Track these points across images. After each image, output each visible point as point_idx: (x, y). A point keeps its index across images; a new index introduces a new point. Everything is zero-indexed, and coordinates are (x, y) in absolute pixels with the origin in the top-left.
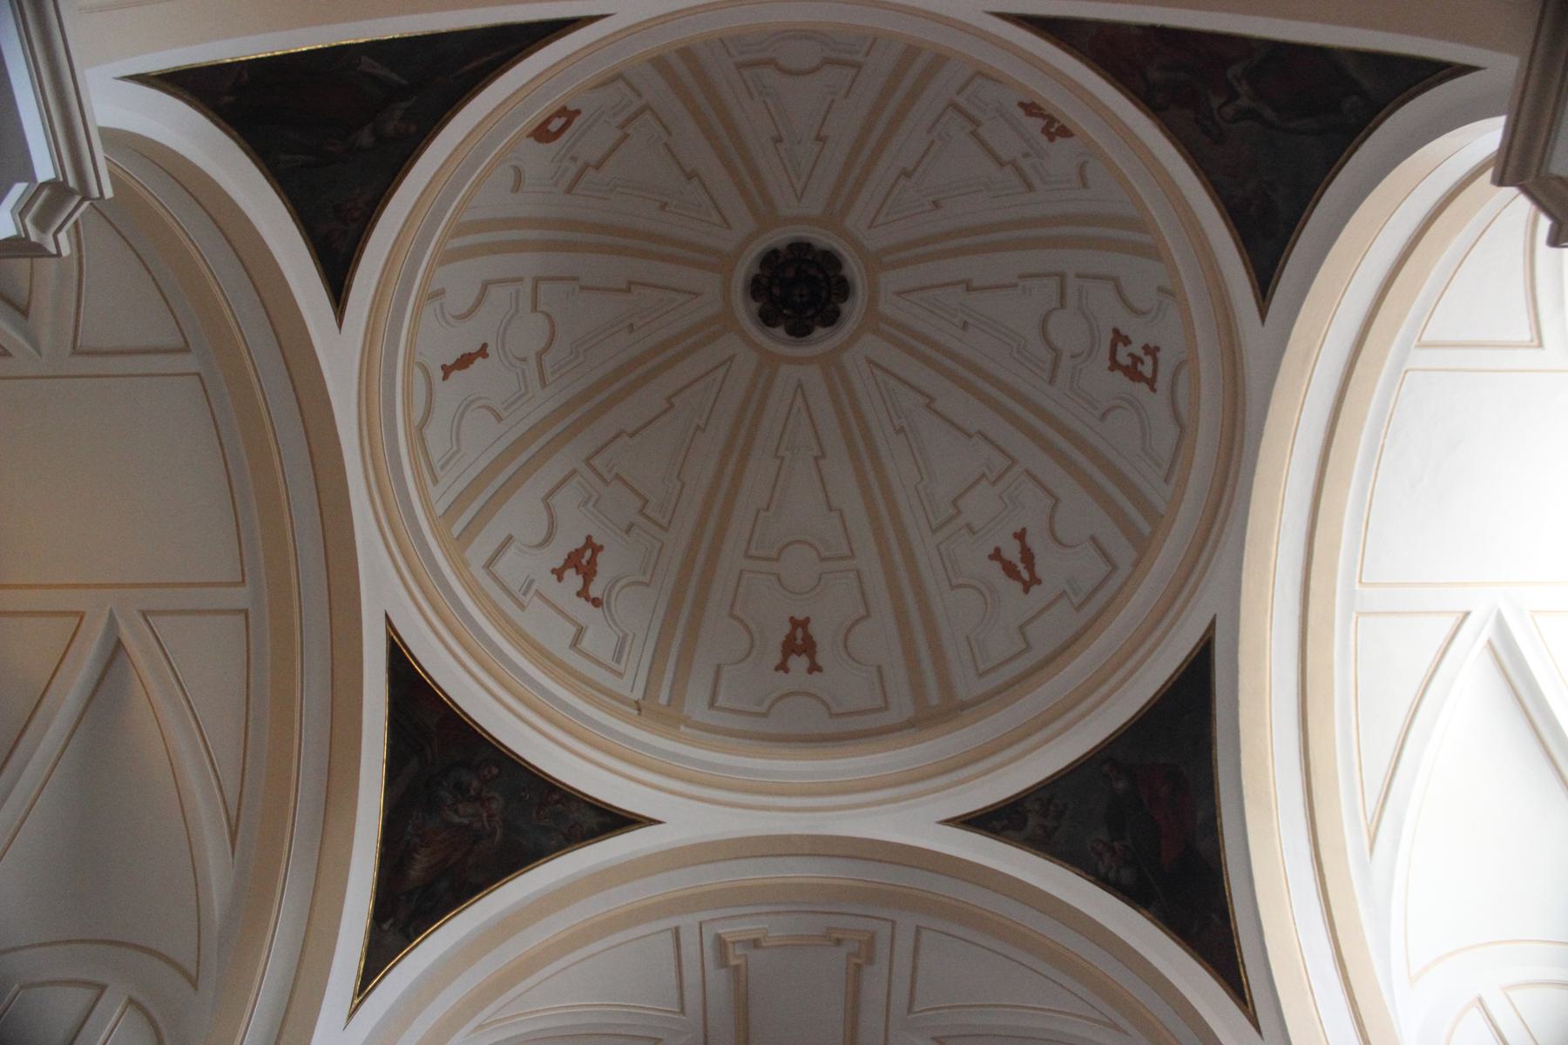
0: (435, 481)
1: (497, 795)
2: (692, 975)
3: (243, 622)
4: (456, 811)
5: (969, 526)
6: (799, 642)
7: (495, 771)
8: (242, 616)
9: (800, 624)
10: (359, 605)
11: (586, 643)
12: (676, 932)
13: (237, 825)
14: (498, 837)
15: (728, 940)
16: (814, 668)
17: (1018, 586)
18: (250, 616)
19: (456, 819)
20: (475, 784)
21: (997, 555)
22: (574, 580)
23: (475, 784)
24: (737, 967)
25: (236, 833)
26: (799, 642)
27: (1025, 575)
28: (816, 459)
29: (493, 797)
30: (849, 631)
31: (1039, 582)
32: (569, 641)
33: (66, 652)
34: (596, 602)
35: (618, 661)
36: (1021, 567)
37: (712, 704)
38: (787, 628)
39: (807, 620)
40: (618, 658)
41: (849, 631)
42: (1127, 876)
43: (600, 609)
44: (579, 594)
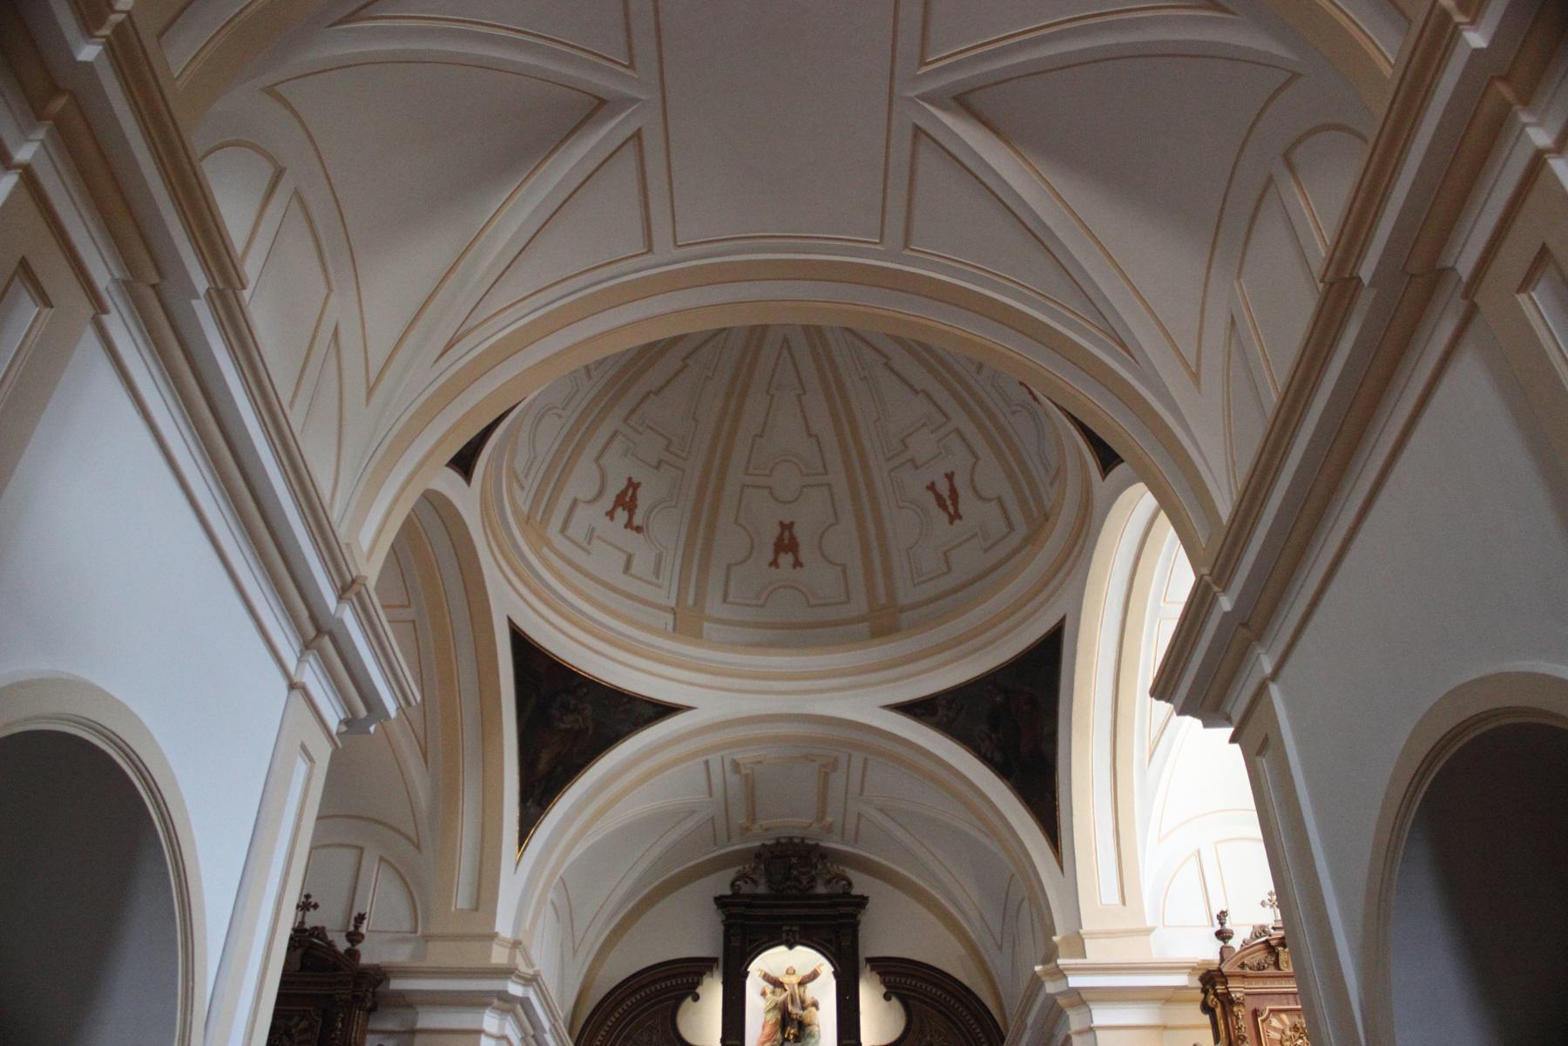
0: (522, 488)
2: (717, 779)
5: (912, 460)
6: (786, 541)
7: (585, 690)
9: (787, 527)
11: (635, 569)
12: (707, 763)
14: (590, 732)
15: (741, 763)
16: (797, 564)
17: (946, 518)
18: (417, 624)
20: (573, 702)
21: (932, 487)
22: (621, 515)
23: (573, 702)
24: (747, 775)
25: (426, 751)
26: (786, 541)
27: (951, 510)
28: (799, 396)
30: (821, 537)
31: (960, 517)
32: (621, 568)
34: (639, 529)
35: (658, 577)
36: (949, 502)
37: (725, 599)
38: (777, 530)
39: (792, 524)
40: (657, 573)
41: (821, 537)
42: (998, 756)
43: (641, 535)
44: (626, 527)
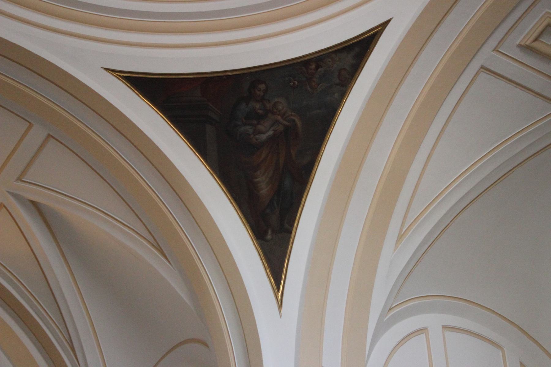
1: (276, 100)
3: (54, 140)
4: (260, 133)
7: (262, 87)
8: (52, 141)
10: (84, 85)
13: (161, 248)
15: (528, 43)
19: (264, 137)
20: (258, 106)
29: (276, 103)
33: (22, 232)
